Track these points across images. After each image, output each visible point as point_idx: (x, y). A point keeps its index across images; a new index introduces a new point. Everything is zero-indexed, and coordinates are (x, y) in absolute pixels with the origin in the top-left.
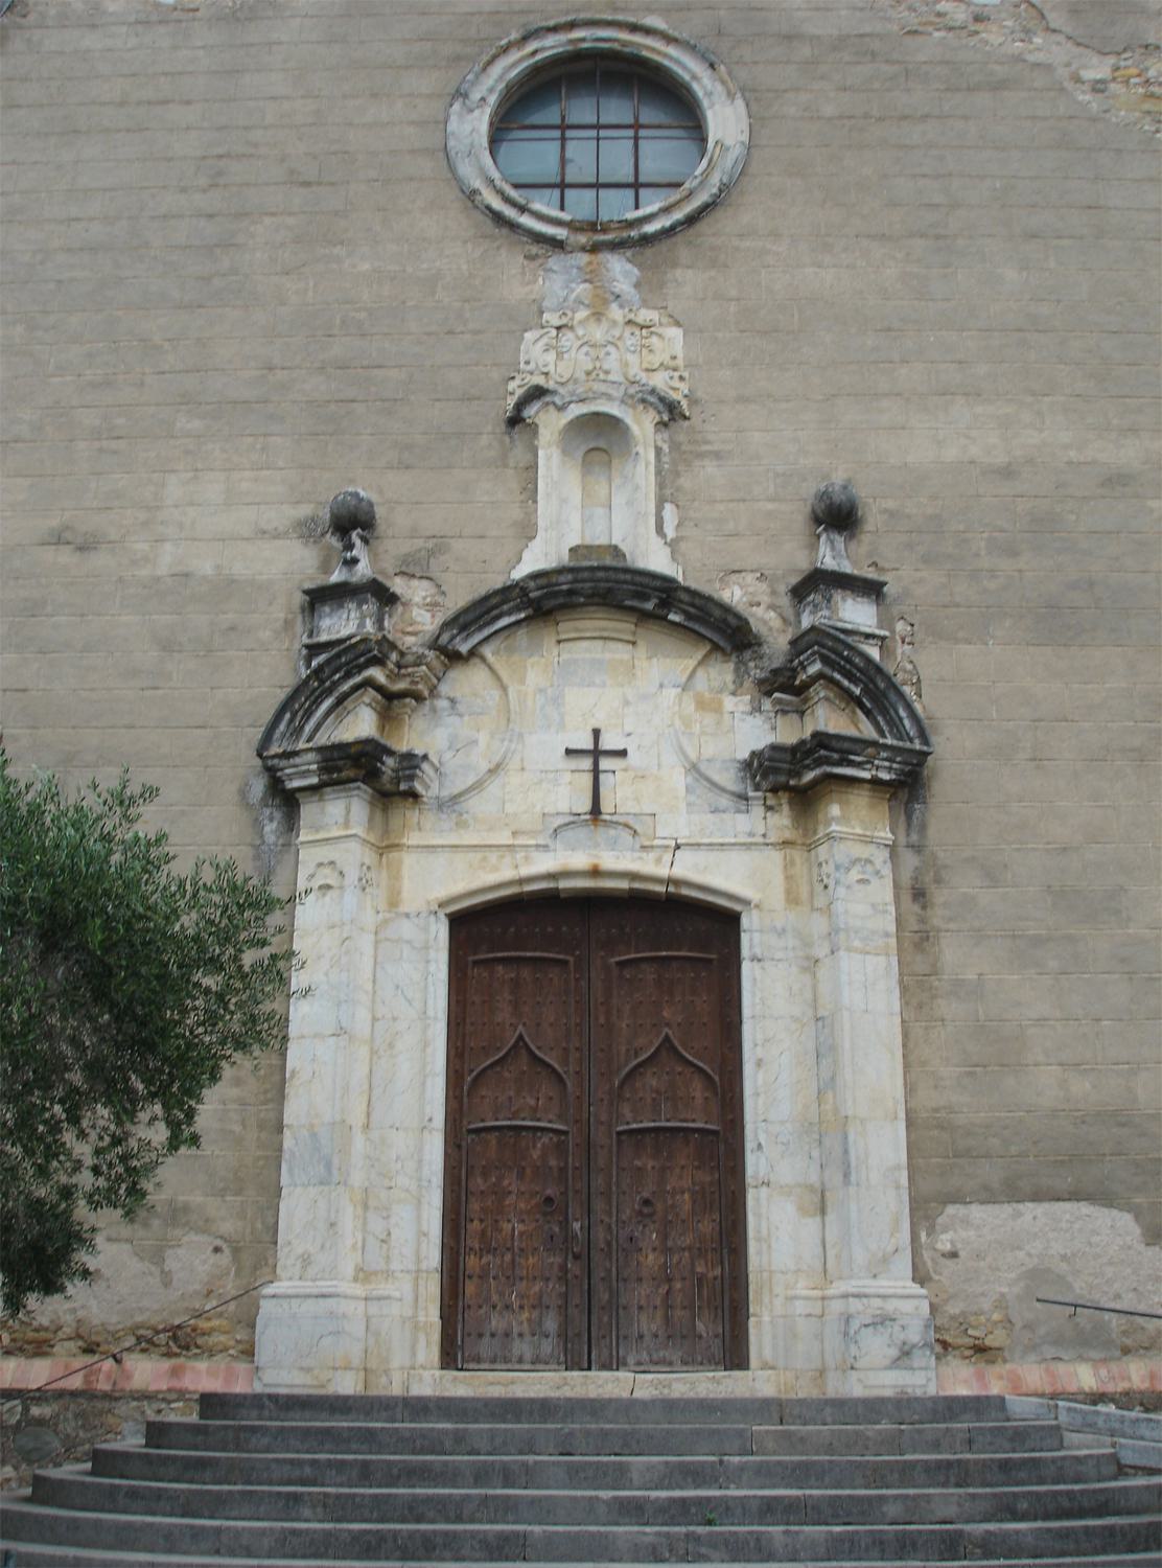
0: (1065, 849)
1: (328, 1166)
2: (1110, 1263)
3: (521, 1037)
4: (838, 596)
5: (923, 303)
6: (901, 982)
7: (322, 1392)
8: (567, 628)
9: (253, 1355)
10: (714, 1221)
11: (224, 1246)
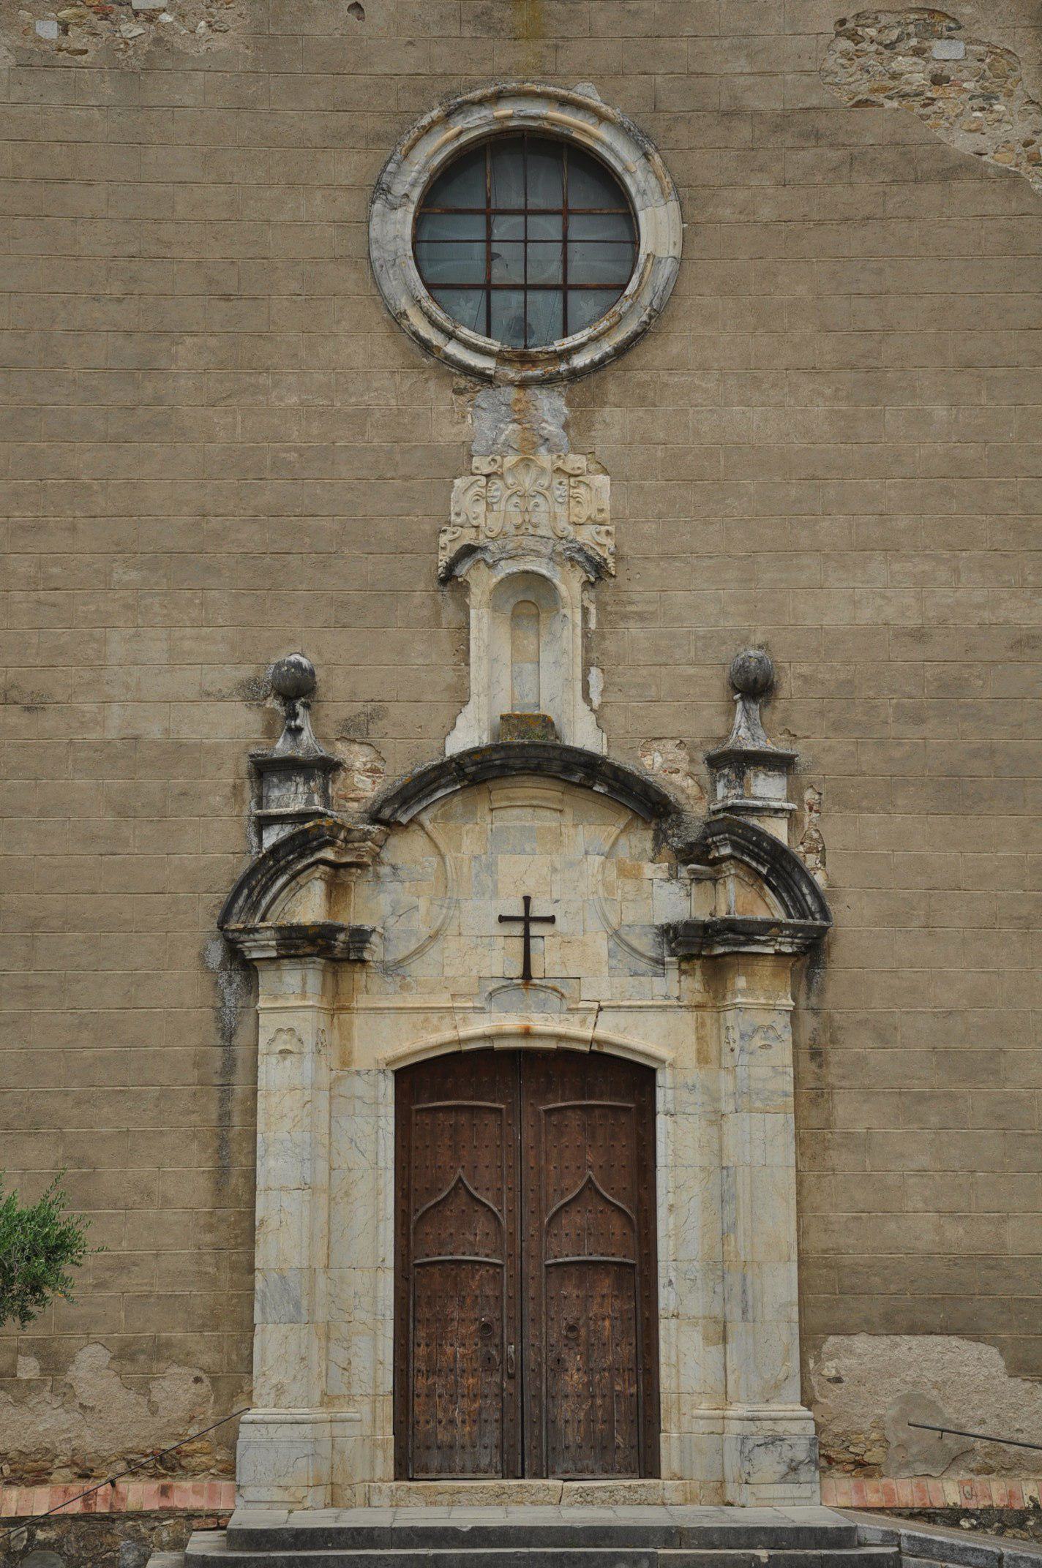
0: (951, 1013)
1: (297, 1305)
3: (460, 1180)
5: (849, 446)
6: (797, 1135)
9: (234, 1472)
10: (631, 1344)
11: (204, 1376)
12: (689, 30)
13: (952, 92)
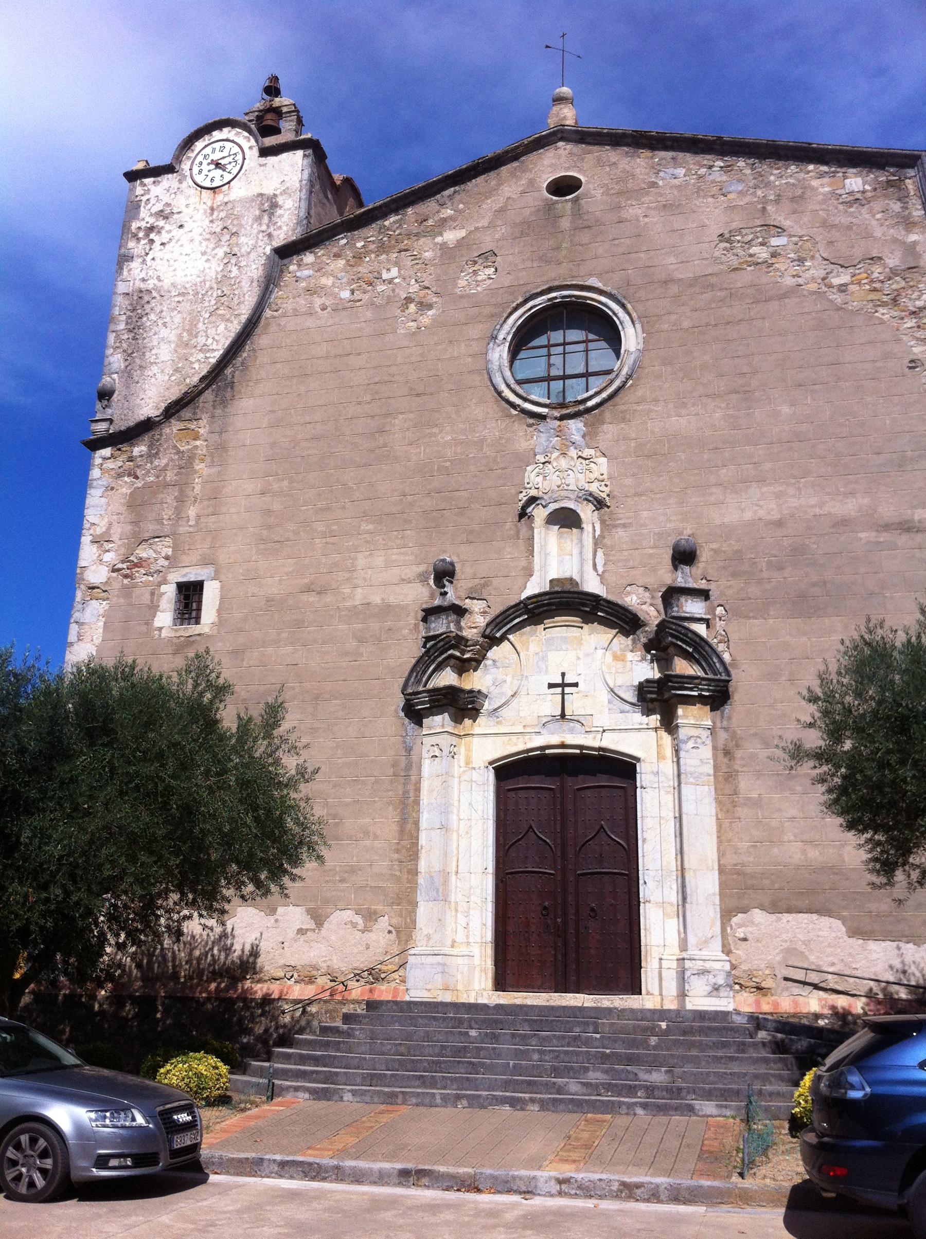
2: (829, 946)
4: (683, 599)
7: (435, 1000)
8: (548, 622)
12: (645, 248)
13: (781, 260)
